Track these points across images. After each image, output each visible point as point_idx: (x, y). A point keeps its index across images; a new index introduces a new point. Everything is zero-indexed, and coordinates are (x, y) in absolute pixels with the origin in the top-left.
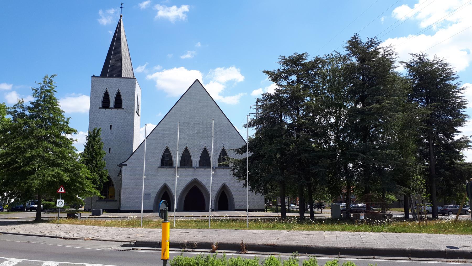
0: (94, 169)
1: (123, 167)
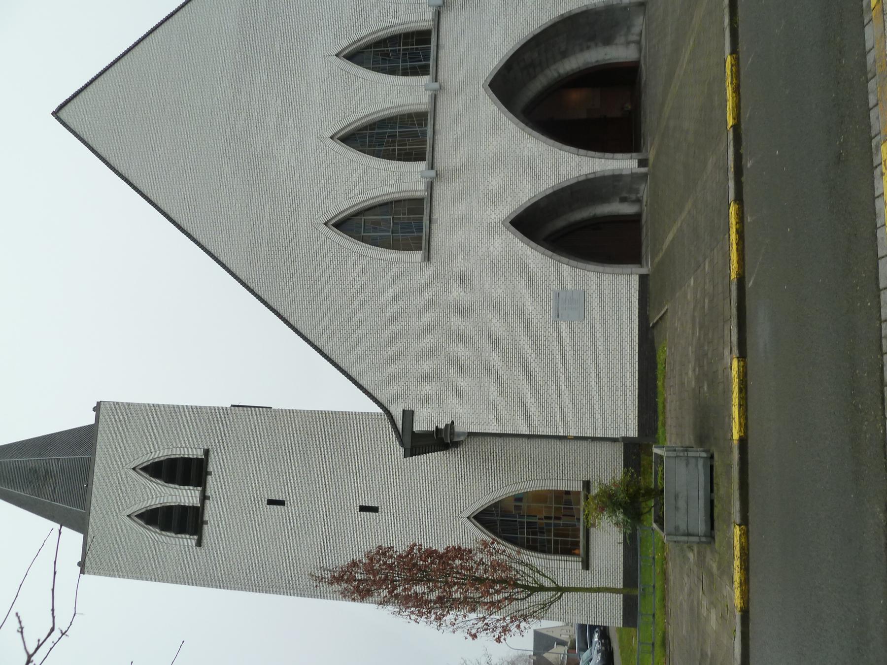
0: (446, 582)
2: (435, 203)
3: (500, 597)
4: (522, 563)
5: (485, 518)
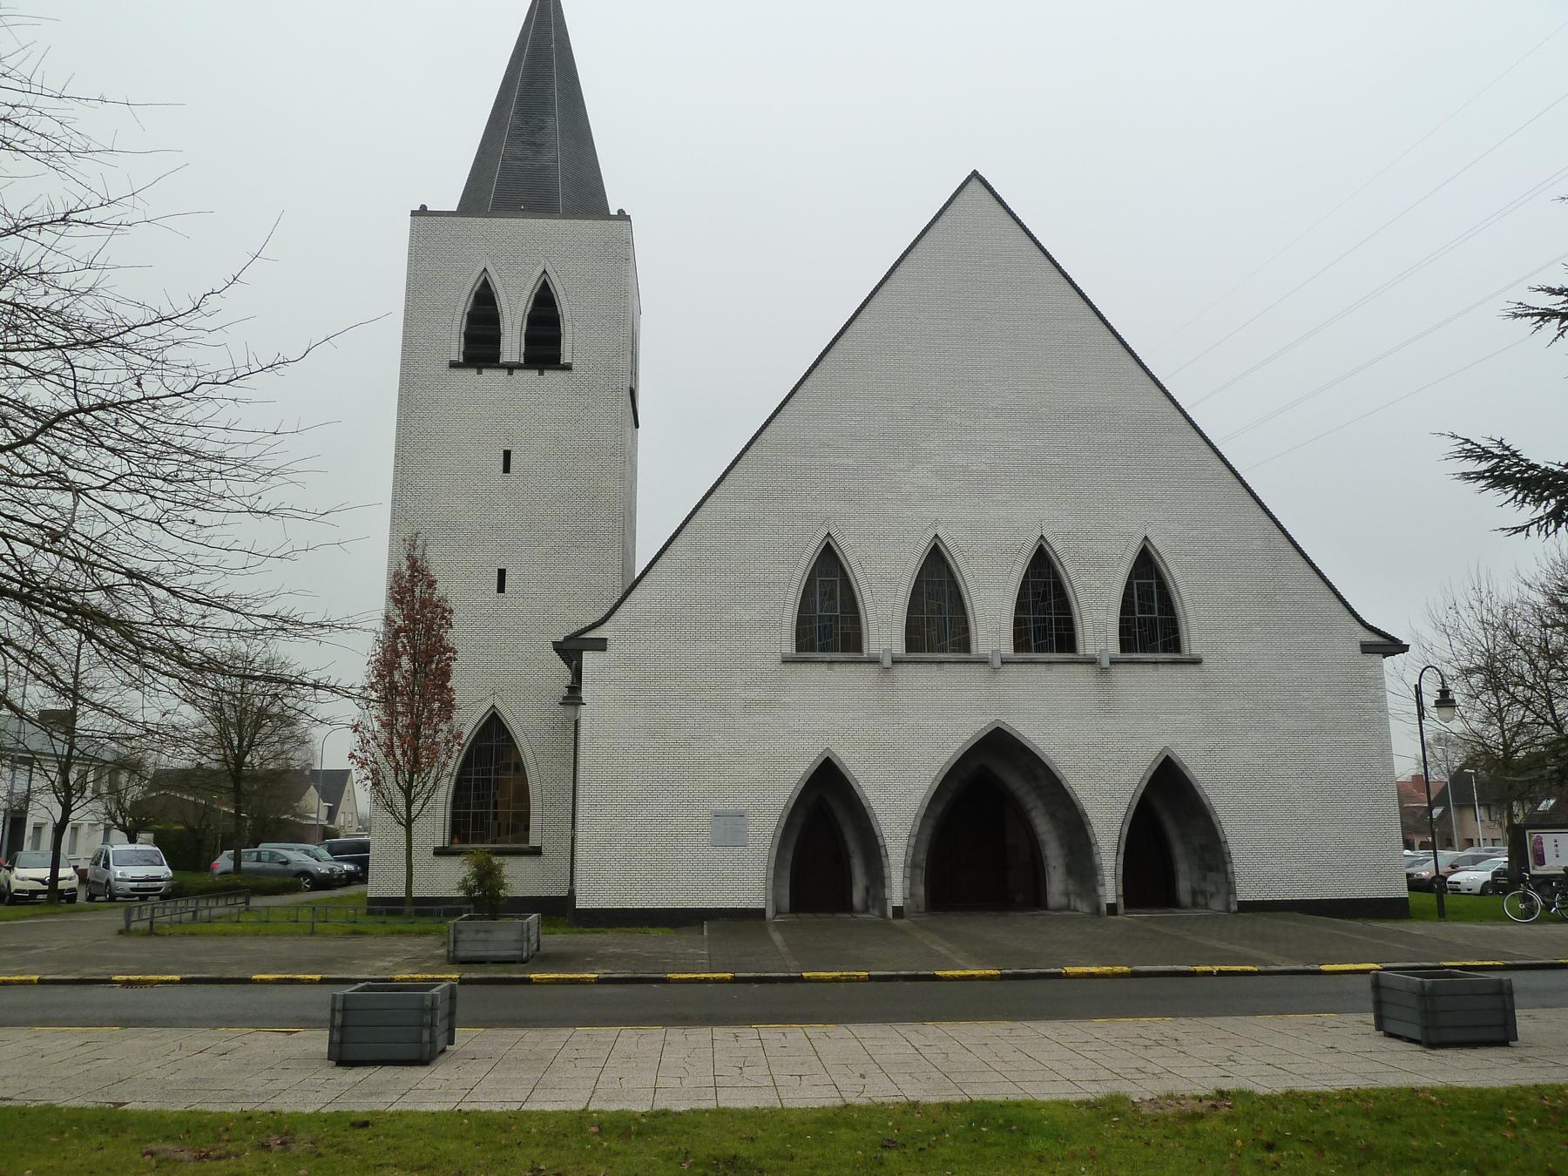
2: (852, 667)
3: (399, 757)
4: (437, 780)
5: (494, 728)
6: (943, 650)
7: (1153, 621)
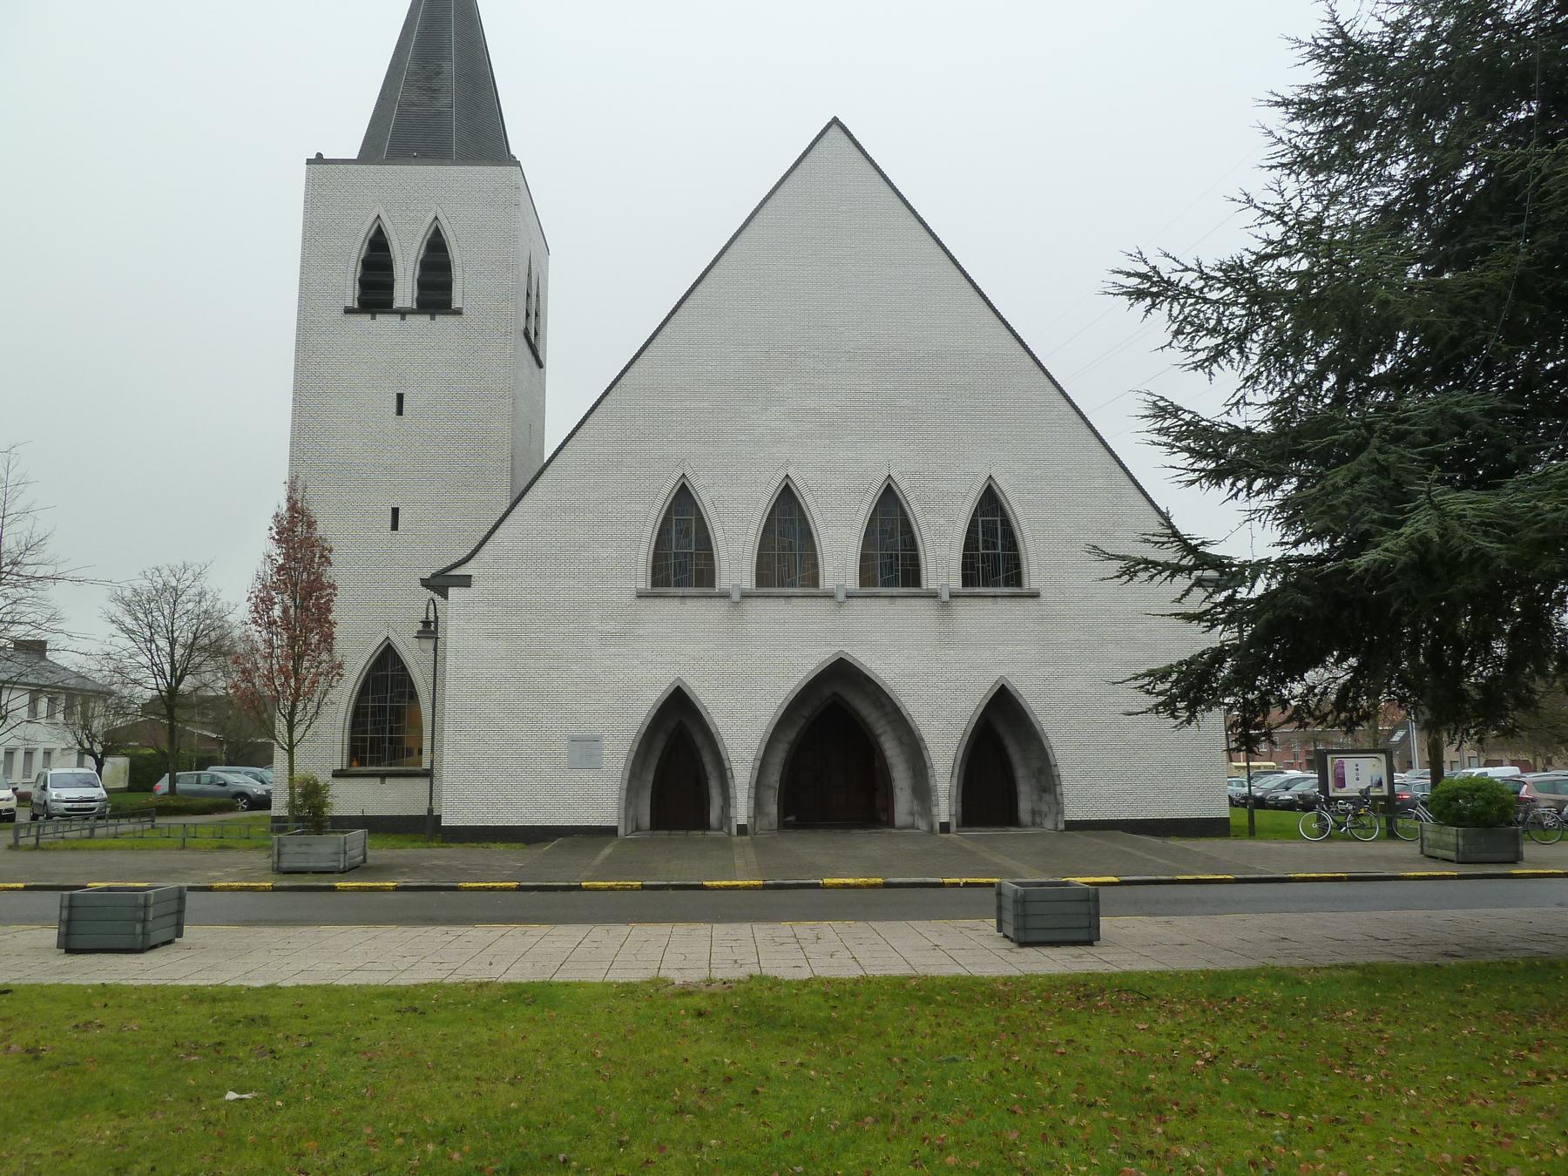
1: (452, 591)
5: (387, 658)
6: (792, 585)
7: (996, 556)
